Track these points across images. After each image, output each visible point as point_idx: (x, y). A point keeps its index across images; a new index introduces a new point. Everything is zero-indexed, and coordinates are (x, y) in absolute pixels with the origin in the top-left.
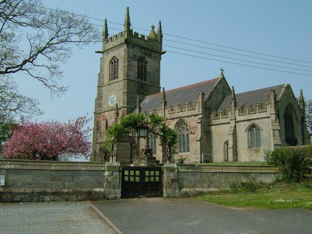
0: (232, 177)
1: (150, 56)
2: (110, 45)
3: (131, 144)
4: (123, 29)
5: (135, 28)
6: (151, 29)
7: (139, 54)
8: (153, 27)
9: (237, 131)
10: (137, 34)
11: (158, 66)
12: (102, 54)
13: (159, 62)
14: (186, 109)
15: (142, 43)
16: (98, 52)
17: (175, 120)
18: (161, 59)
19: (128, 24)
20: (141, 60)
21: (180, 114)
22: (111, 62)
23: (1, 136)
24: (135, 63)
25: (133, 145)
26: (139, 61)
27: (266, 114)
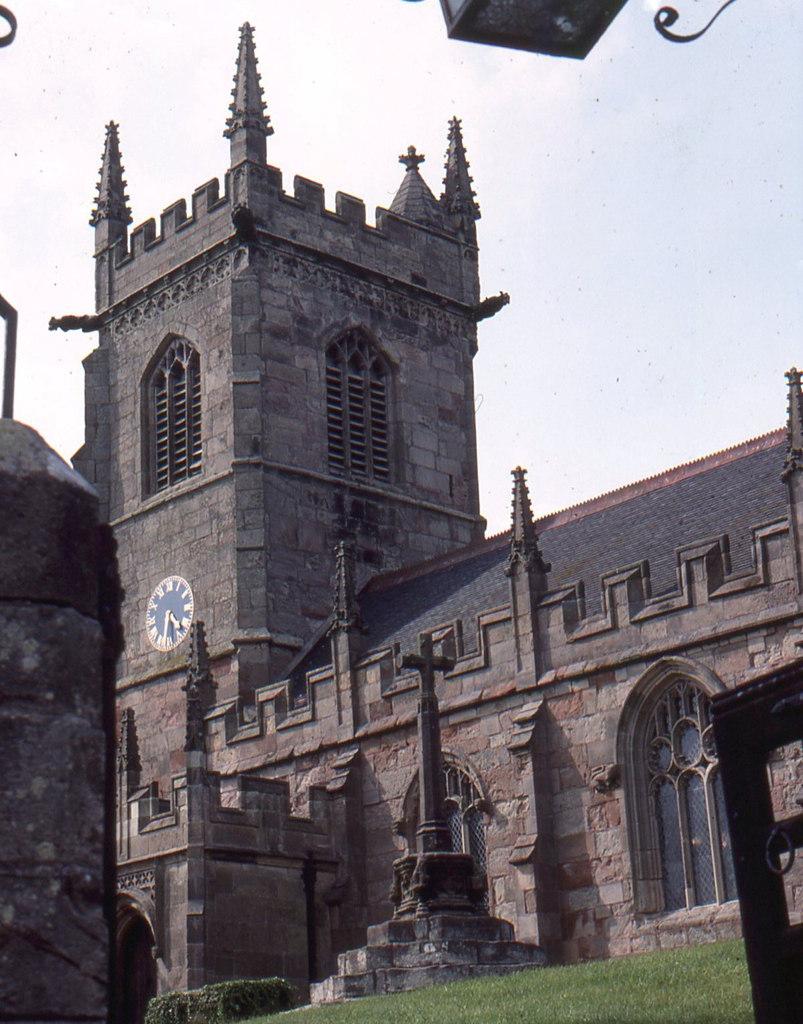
0: (665, 801)
1: (405, 326)
2: (146, 270)
3: (309, 877)
4: (216, 160)
5: (289, 156)
6: (401, 172)
7: (335, 312)
8: (412, 160)
9: (288, 644)
10: (310, 190)
11: (459, 387)
12: (95, 334)
13: (466, 370)
14: (701, 591)
15: (345, 245)
16: (68, 323)
17: (620, 675)
18: (474, 349)
19: (250, 123)
20: (350, 349)
21: (659, 636)
22: (152, 378)
23: (1, 749)
24: (312, 364)
25: (324, 880)
26: (333, 353)
27: (674, 630)
